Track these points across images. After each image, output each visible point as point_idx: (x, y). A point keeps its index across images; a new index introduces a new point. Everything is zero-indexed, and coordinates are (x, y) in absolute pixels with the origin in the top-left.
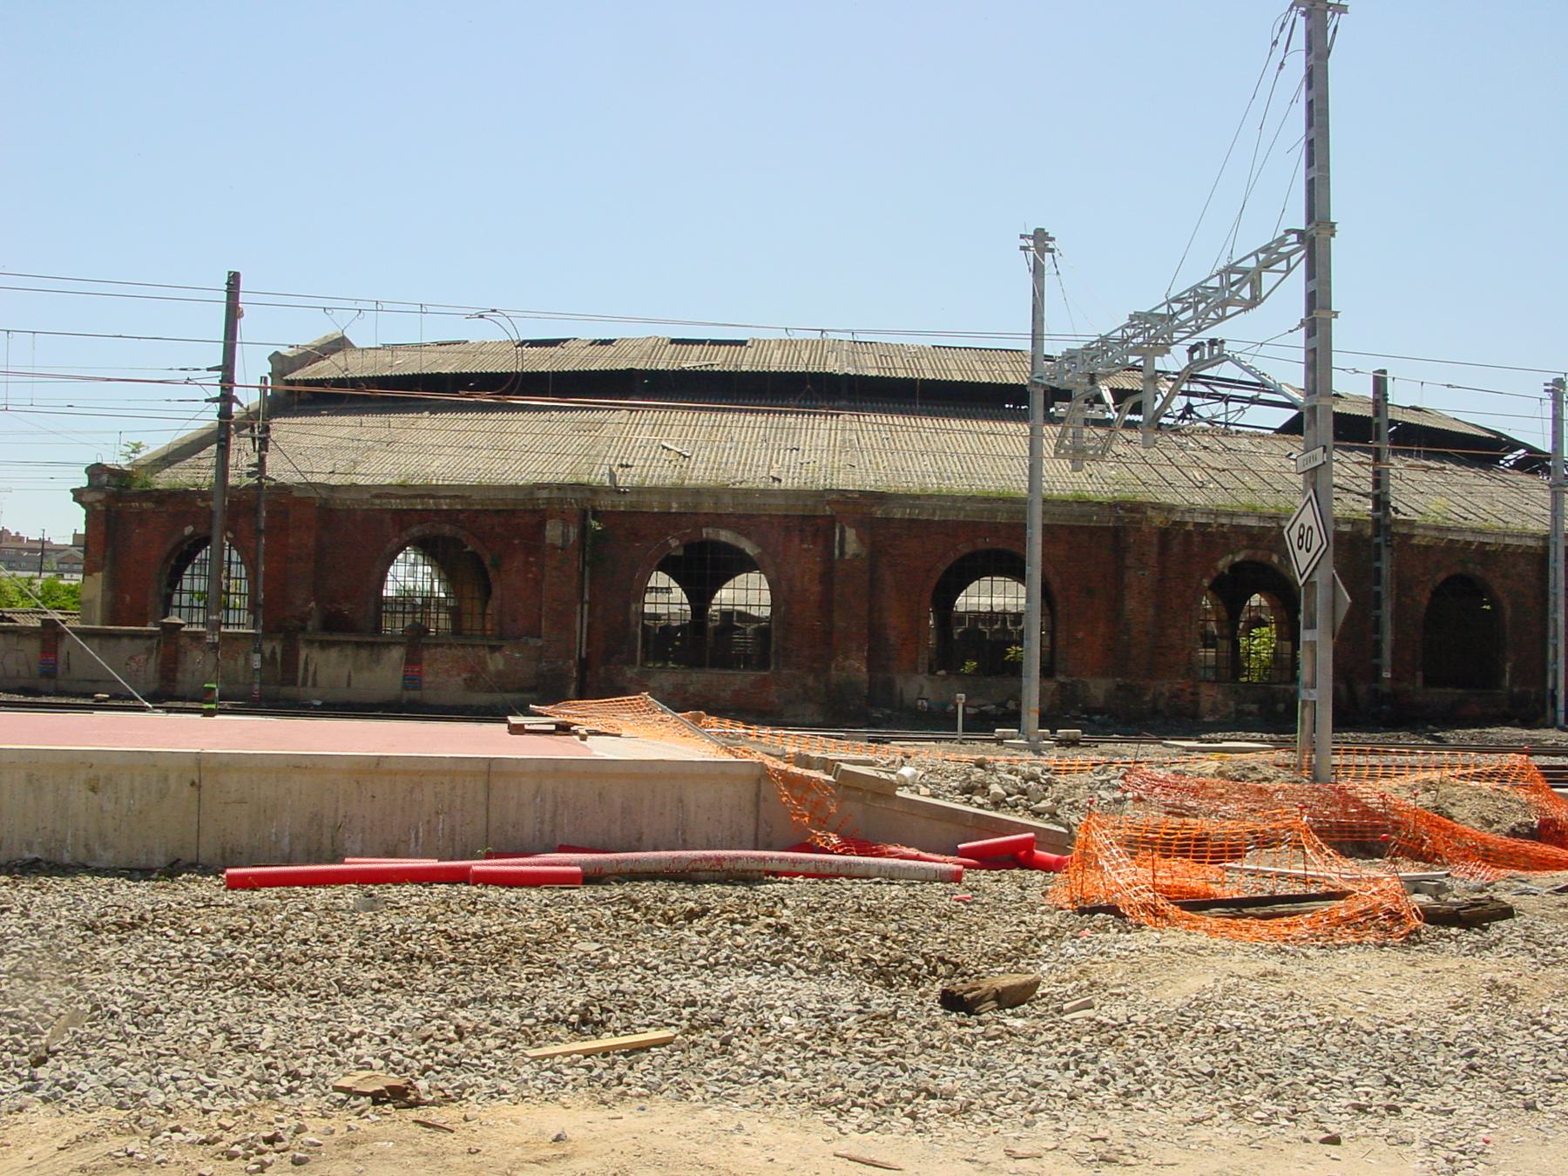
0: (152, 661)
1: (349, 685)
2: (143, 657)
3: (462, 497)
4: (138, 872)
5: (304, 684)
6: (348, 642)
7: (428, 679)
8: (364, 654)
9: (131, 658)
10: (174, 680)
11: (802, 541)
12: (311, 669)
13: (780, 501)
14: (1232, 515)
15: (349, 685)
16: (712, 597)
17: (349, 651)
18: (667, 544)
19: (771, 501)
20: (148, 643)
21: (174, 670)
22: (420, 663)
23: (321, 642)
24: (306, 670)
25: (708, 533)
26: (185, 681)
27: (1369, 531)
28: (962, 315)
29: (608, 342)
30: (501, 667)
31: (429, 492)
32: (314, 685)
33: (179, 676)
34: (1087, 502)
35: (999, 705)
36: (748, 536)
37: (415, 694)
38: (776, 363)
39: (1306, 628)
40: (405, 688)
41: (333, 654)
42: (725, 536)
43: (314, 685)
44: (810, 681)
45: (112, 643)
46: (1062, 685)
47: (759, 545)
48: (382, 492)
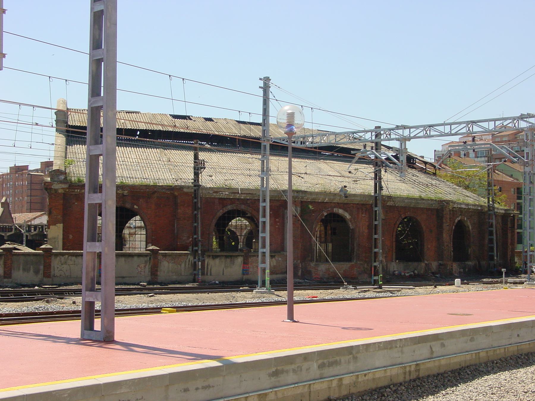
0: (147, 267)
1: (223, 274)
2: (143, 265)
3: (252, 194)
4: (429, 359)
5: (207, 274)
6: (222, 256)
7: (251, 270)
8: (228, 260)
9: (138, 266)
10: (157, 275)
11: (362, 214)
12: (209, 268)
13: (359, 198)
14: (458, 204)
15: (223, 274)
16: (127, 222)
17: (223, 260)
18: (323, 214)
19: (356, 198)
20: (146, 259)
21: (157, 271)
22: (248, 264)
23: (213, 256)
24: (207, 267)
25: (335, 210)
26: (162, 275)
27: (486, 209)
28: (230, 108)
29: (210, 120)
30: (275, 264)
31: (234, 191)
32: (211, 275)
33: (159, 273)
34: (432, 200)
35: (414, 272)
36: (347, 211)
37: (245, 277)
38: (226, 132)
39: (262, 232)
40: (243, 274)
41: (217, 261)
42: (341, 211)
43: (211, 275)
44: (366, 266)
45: (130, 259)
46: (426, 264)
47: (350, 214)
48: (216, 190)
